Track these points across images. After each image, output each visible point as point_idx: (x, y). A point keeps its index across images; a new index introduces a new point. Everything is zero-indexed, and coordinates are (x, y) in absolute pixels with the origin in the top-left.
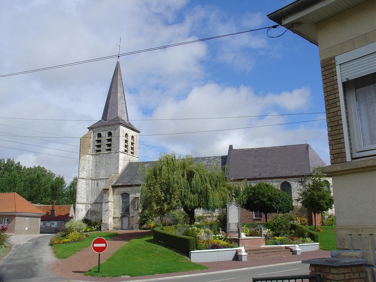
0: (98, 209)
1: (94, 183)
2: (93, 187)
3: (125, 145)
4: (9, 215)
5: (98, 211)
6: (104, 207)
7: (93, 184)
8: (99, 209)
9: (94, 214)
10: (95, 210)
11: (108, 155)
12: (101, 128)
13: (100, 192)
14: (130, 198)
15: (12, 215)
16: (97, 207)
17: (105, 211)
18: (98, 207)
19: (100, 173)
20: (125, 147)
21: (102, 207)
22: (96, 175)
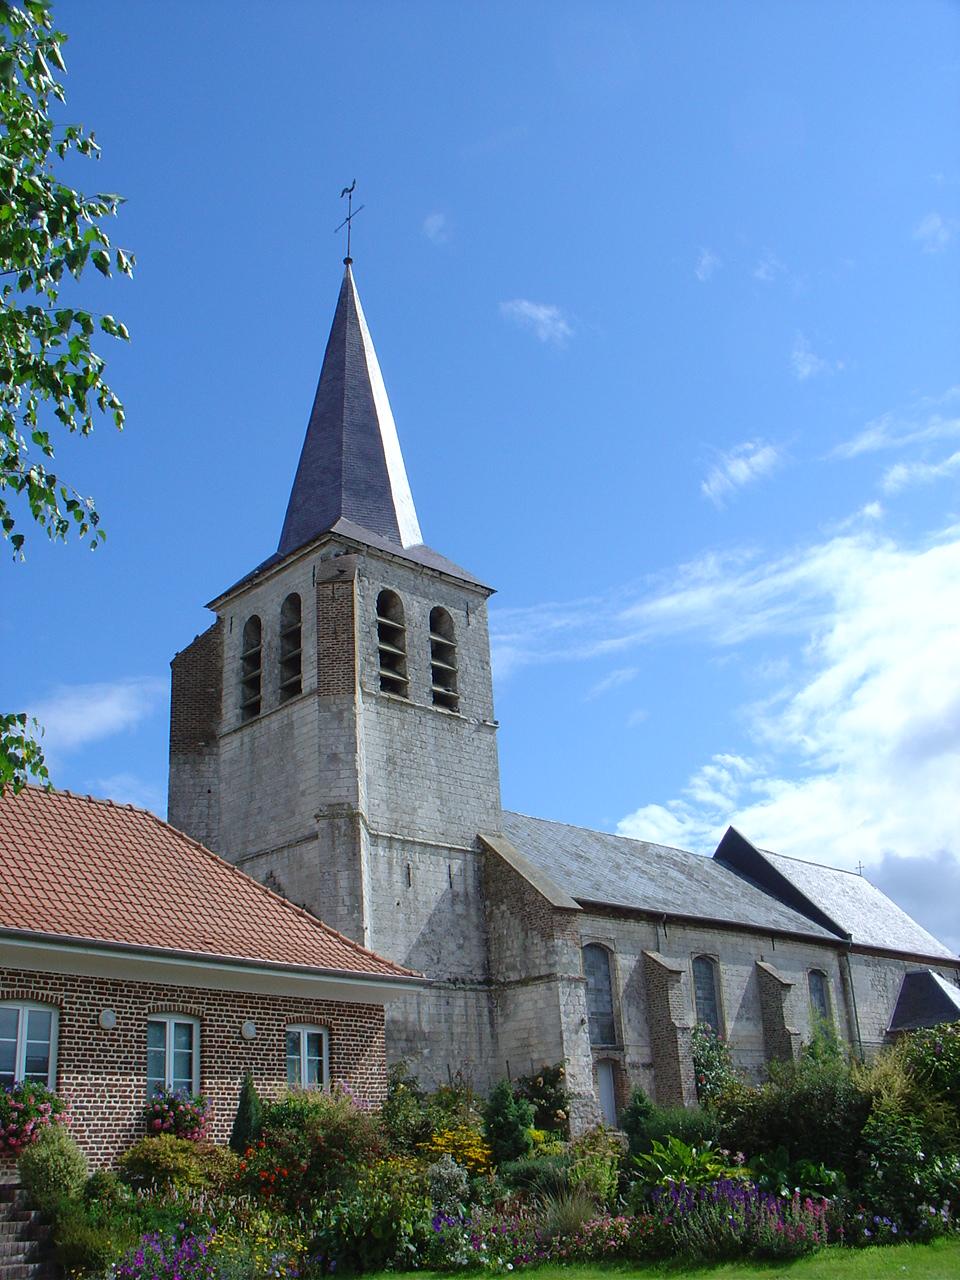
0: (425, 1018)
1: (390, 864)
2: (384, 884)
3: (383, 653)
4: (330, 1004)
5: (426, 1028)
6: (567, 1004)
7: (383, 867)
8: (429, 1022)
9: (403, 1044)
10: (406, 1021)
11: (445, 726)
12: (400, 572)
13: (426, 921)
14: (620, 974)
15: (360, 1006)
16: (418, 1004)
17: (572, 1027)
18: (425, 1008)
19: (415, 809)
20: (383, 665)
21: (558, 1006)
22: (395, 816)
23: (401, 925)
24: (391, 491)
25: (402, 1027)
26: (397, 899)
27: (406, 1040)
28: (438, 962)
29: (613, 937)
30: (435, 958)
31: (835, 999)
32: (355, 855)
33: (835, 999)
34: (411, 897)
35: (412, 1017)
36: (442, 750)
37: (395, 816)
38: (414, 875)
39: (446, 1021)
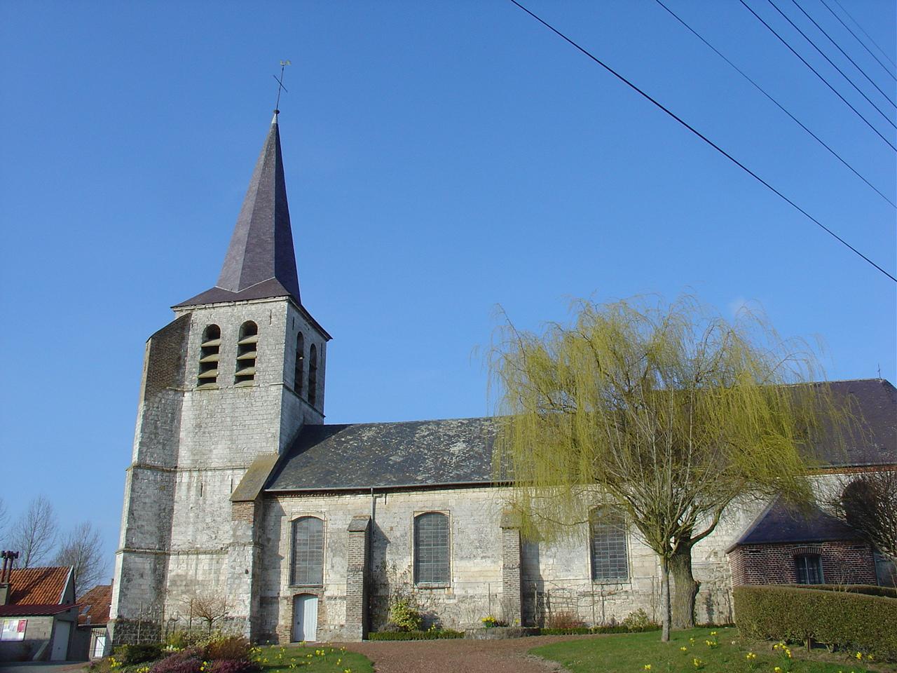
0: (200, 572)
5: (200, 578)
9: (183, 588)
19: (211, 451)
23: (191, 520)
24: (43, 665)
25: (184, 578)
26: (191, 505)
27: (185, 586)
28: (215, 539)
29: (323, 510)
30: (214, 536)
31: (306, 368)
32: (173, 420)
33: (306, 368)
34: (201, 502)
35: (191, 573)
36: (237, 410)
37: (196, 458)
38: (206, 489)
39: (215, 573)
